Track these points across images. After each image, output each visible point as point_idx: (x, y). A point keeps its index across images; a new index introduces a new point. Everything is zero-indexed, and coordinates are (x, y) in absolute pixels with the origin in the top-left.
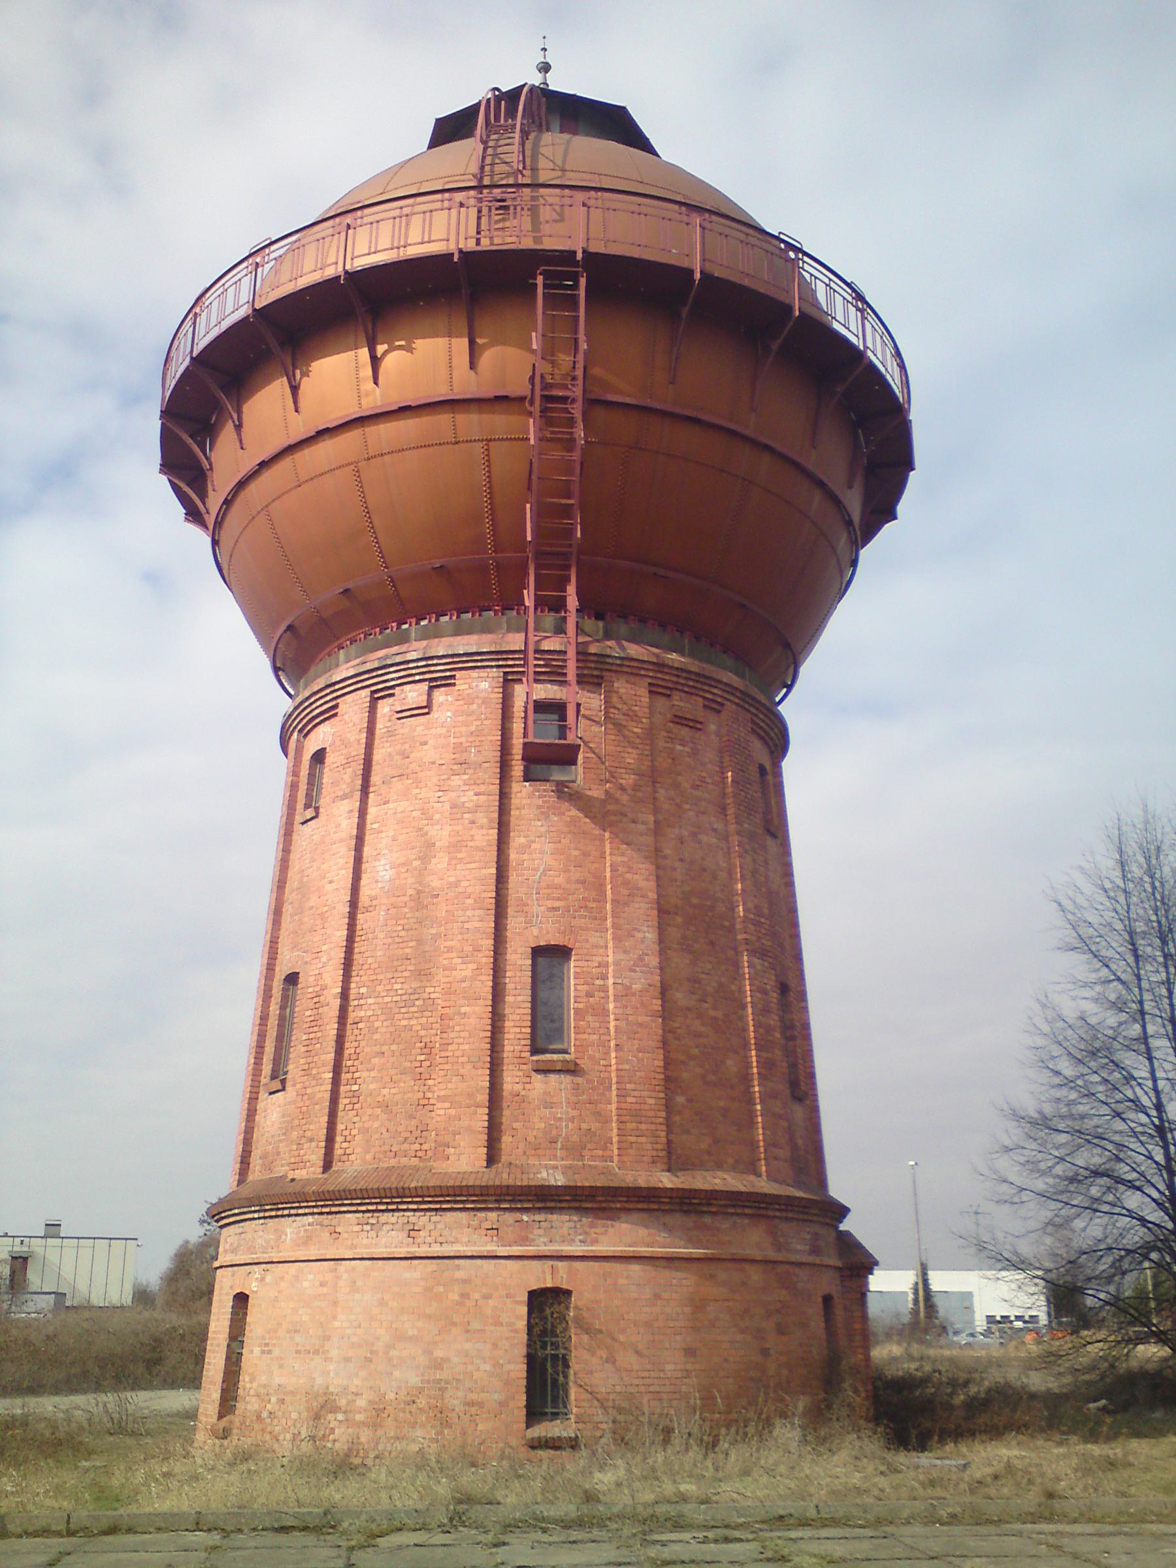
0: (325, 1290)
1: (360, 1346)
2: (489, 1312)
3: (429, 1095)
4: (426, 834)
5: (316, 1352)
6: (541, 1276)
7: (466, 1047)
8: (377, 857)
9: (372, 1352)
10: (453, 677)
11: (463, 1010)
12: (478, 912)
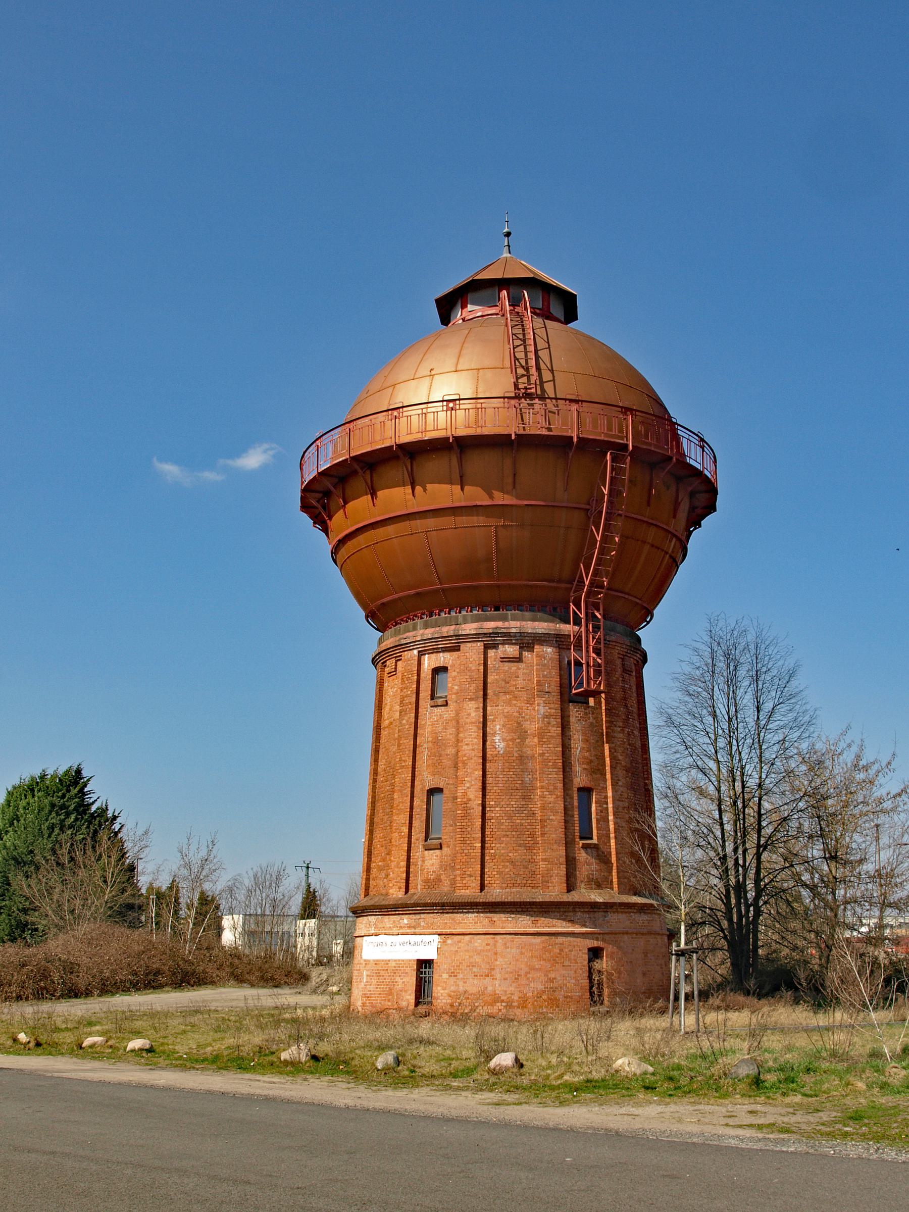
0: (489, 947)
1: (512, 973)
3: (535, 857)
5: (487, 976)
8: (494, 734)
10: (401, 656)
12: (554, 770)
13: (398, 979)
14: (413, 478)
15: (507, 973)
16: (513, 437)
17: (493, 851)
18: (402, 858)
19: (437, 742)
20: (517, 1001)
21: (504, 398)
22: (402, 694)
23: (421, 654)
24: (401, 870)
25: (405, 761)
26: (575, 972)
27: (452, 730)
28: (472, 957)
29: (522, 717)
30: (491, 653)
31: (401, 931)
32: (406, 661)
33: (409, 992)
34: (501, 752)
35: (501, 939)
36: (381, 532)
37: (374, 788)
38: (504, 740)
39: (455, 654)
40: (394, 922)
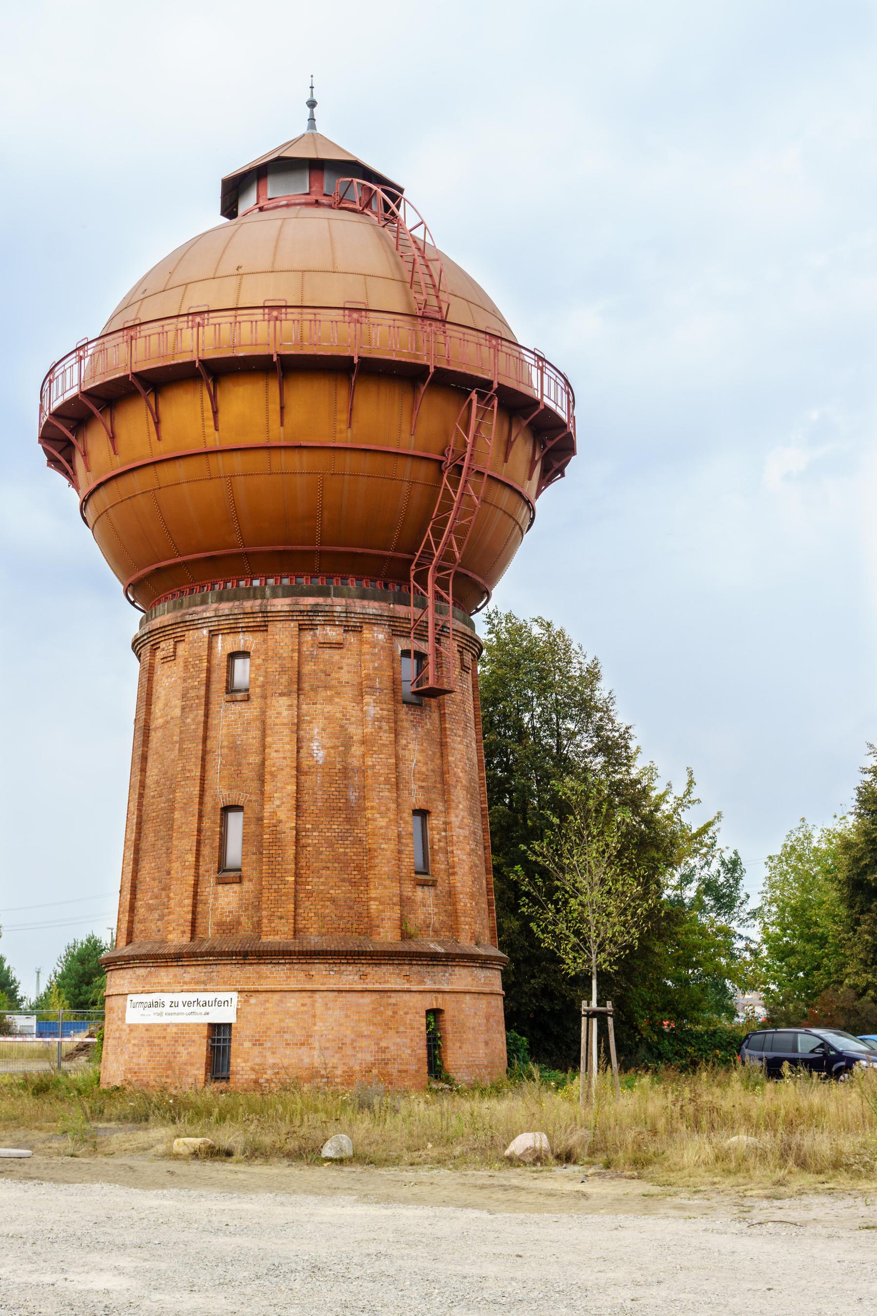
0: (305, 1008)
1: (334, 1040)
2: (408, 1022)
3: (362, 896)
4: (347, 730)
5: (302, 1044)
6: (431, 1002)
7: (386, 869)
8: (311, 740)
9: (343, 1044)
11: (383, 846)
12: (387, 786)
13: (180, 1049)
14: (158, 418)
15: (328, 1040)
16: (356, 360)
17: (310, 887)
18: (186, 894)
19: (236, 749)
20: (341, 1076)
21: (344, 309)
22: (185, 685)
23: (213, 634)
24: (186, 909)
25: (190, 771)
26: (412, 1040)
27: (255, 733)
28: (280, 1020)
29: (346, 719)
30: (308, 637)
31: (185, 987)
32: (190, 642)
33: (198, 1065)
34: (321, 762)
35: (321, 997)
36: (167, 473)
37: (140, 805)
38: (324, 747)
39: (259, 636)
40: (175, 976)
